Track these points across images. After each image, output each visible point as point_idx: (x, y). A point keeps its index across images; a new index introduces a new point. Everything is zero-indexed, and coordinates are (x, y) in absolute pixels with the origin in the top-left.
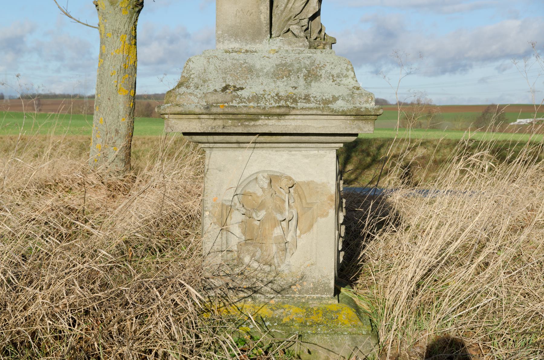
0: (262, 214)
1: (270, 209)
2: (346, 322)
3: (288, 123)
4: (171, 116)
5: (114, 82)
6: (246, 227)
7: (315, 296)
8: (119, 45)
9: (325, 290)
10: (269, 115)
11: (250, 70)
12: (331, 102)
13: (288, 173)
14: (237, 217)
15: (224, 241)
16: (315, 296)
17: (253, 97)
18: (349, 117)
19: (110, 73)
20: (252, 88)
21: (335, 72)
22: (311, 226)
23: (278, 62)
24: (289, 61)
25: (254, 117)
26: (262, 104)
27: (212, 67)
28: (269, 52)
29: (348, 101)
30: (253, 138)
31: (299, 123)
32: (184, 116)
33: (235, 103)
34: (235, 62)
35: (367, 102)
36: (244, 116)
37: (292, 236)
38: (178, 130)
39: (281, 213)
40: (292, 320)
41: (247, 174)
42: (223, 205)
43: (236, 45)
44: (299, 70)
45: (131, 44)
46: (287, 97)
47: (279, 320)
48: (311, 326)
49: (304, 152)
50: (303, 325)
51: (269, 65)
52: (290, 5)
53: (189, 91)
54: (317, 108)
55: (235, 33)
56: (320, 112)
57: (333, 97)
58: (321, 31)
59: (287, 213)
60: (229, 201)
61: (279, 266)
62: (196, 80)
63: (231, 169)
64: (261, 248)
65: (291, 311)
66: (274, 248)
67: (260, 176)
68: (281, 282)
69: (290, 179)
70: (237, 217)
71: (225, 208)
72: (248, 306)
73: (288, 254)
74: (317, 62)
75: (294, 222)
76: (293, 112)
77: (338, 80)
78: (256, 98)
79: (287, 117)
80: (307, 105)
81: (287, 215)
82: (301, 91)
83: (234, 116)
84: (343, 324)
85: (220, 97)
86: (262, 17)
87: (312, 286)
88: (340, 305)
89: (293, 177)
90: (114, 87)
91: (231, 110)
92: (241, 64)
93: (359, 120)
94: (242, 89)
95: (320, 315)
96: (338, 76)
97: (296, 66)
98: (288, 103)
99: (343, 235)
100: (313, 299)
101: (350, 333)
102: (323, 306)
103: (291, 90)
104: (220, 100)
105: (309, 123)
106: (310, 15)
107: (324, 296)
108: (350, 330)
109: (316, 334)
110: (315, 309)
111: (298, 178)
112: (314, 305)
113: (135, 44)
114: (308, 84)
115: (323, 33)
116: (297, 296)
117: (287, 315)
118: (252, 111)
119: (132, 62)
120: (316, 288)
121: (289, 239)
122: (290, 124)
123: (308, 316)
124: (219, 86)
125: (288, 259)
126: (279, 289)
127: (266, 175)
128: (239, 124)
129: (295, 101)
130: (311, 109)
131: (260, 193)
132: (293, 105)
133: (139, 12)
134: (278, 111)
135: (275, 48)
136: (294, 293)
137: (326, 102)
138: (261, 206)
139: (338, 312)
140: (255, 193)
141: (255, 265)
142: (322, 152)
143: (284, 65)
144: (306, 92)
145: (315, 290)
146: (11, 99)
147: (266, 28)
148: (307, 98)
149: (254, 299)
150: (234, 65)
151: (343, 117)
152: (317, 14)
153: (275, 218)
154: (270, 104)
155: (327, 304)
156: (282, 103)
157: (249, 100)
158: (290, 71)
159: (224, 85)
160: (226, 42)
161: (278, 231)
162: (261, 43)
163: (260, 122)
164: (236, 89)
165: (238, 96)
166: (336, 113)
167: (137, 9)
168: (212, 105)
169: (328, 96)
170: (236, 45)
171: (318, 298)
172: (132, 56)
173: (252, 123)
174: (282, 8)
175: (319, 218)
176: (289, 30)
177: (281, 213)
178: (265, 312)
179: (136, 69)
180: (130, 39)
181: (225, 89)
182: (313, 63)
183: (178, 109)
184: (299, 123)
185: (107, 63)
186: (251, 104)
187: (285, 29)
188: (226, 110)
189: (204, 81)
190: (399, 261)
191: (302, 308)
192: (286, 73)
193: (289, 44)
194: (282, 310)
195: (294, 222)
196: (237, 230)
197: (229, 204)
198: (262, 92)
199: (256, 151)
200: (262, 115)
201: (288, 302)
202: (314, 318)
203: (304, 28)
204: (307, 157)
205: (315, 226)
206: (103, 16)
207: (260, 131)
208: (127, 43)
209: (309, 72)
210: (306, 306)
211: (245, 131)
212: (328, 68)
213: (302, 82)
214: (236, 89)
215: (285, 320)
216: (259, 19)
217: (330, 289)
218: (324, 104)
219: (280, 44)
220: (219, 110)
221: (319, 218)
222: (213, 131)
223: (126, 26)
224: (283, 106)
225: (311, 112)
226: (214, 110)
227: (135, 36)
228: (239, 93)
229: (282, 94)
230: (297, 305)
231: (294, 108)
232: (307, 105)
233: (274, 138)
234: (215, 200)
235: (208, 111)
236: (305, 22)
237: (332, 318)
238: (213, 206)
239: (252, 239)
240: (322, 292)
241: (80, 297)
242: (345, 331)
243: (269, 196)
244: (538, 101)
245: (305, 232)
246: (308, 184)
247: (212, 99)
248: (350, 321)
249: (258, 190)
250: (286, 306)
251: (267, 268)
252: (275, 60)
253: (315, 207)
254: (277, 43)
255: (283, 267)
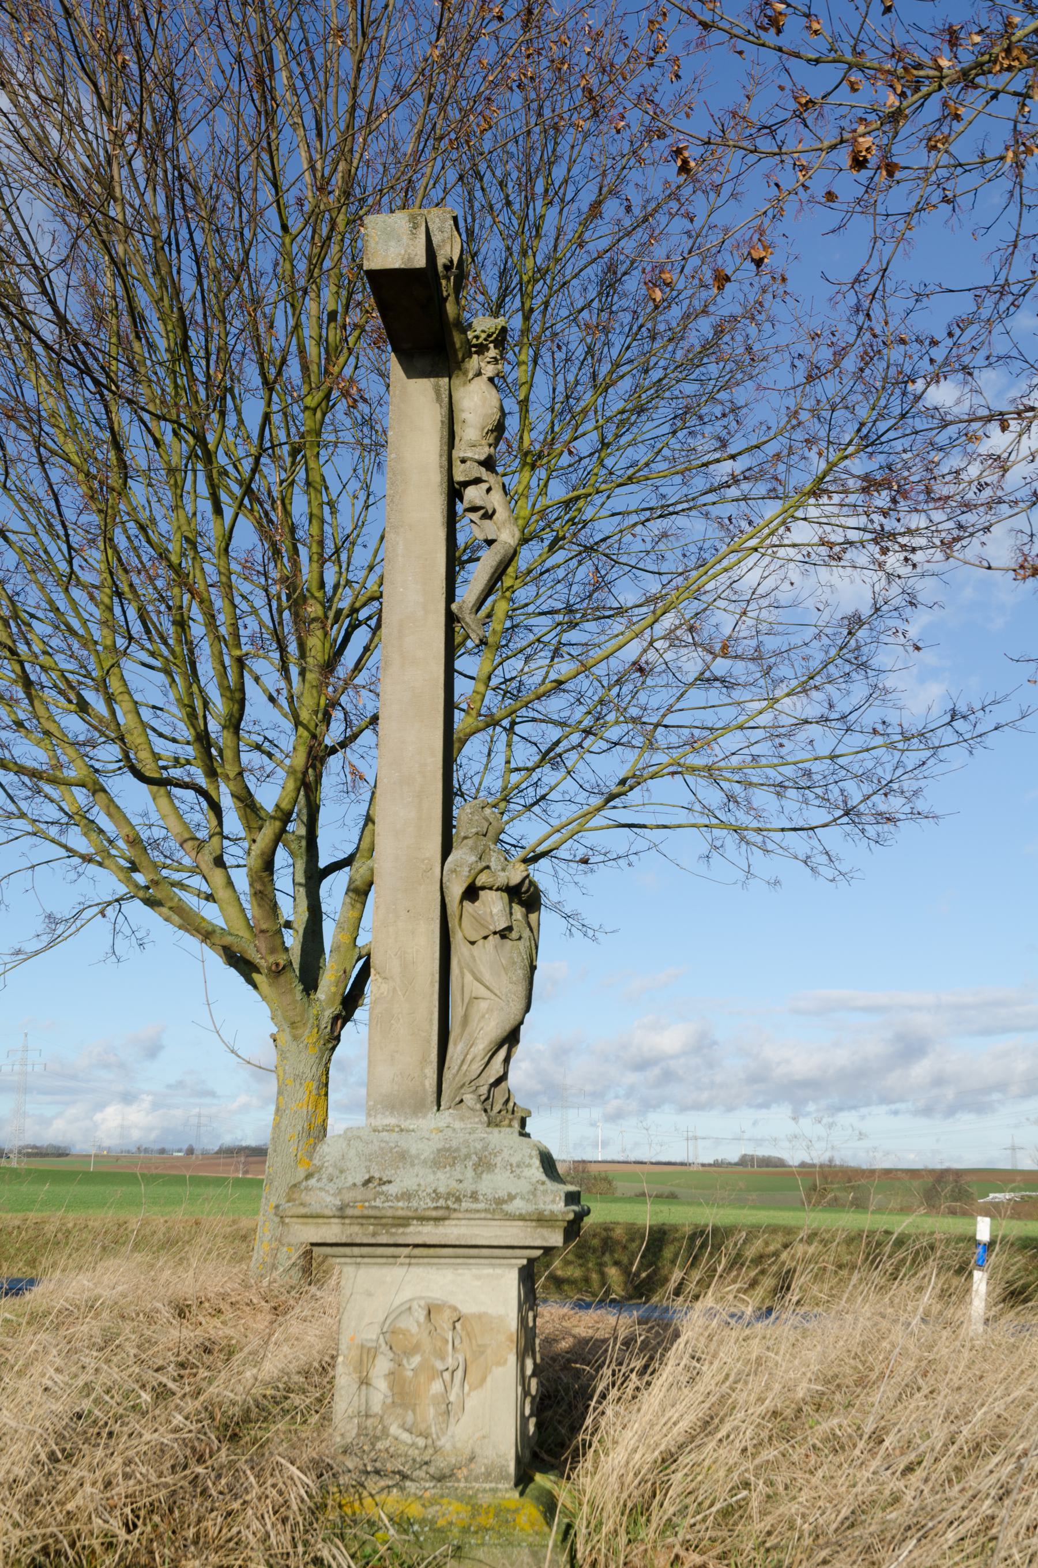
0: (416, 1360)
1: (433, 1354)
2: (527, 1527)
3: (448, 1230)
4: (294, 1220)
5: (292, 1149)
6: (394, 1378)
7: (488, 1486)
8: (303, 1094)
9: (503, 1477)
10: (422, 1219)
11: (403, 1157)
12: (504, 1202)
13: (453, 1301)
14: (382, 1365)
15: (363, 1400)
16: (488, 1486)
17: (403, 1194)
18: (529, 1223)
19: (288, 1137)
20: (404, 1180)
21: (514, 1160)
22: (483, 1379)
23: (440, 1146)
24: (454, 1144)
25: (403, 1222)
26: (414, 1204)
27: (352, 1153)
28: (433, 1129)
29: (528, 1200)
30: (406, 1251)
31: (463, 1230)
32: (310, 1220)
33: (378, 1203)
34: (383, 1145)
35: (553, 1201)
36: (390, 1221)
37: (458, 1395)
38: (302, 1240)
39: (443, 1358)
40: (451, 1523)
41: (397, 1303)
42: (362, 1346)
43: (391, 1121)
44: (467, 1157)
45: (319, 1095)
46: (449, 1194)
47: (433, 1522)
48: (476, 1532)
49: (475, 1271)
50: (465, 1530)
51: (426, 1149)
52: (465, 1067)
53: (319, 1185)
54: (486, 1211)
55: (392, 1104)
56: (490, 1216)
57: (509, 1194)
58: (507, 1101)
59: (450, 1359)
60: (371, 1340)
61: (439, 1438)
62: (330, 1170)
63: (373, 1296)
64: (414, 1411)
65: (451, 1508)
66: (432, 1411)
67: (415, 1305)
68: (440, 1464)
69: (455, 1309)
70: (382, 1365)
71: (365, 1351)
72: (393, 1500)
73: (452, 1420)
74: (491, 1146)
75: (459, 1374)
76: (454, 1215)
77: (518, 1171)
78: (407, 1196)
79: (447, 1222)
80: (475, 1206)
81: (450, 1362)
82: (468, 1186)
83: (378, 1220)
84: (522, 1530)
85: (359, 1194)
86: (427, 1083)
87: (483, 1470)
88: (522, 1500)
89: (460, 1307)
90: (293, 1158)
91: (371, 1212)
92: (392, 1148)
93: (542, 1227)
94: (390, 1182)
95: (491, 1515)
96: (518, 1166)
97: (464, 1151)
98: (449, 1203)
99: (533, 1392)
100: (485, 1491)
101: (530, 1545)
102: (496, 1501)
103: (454, 1184)
104: (359, 1198)
105: (476, 1231)
106: (492, 1080)
107: (500, 1486)
108: (531, 1539)
109: (483, 1544)
110: (485, 1506)
111: (467, 1308)
112: (485, 1499)
113: (326, 1094)
114: (479, 1176)
115: (511, 1104)
116: (462, 1485)
117: (444, 1515)
118: (400, 1213)
119: (320, 1120)
120: (489, 1474)
121: (452, 1398)
122: (451, 1232)
123: (473, 1517)
124: (360, 1178)
125: (451, 1428)
126: (437, 1475)
127: (422, 1303)
128: (385, 1233)
129: (458, 1200)
130: (478, 1211)
131: (414, 1329)
132: (456, 1206)
133: (333, 1049)
134: (434, 1214)
135: (442, 1124)
136: (458, 1480)
137: (500, 1202)
138: (416, 1349)
139: (517, 1511)
140: (409, 1331)
141: (405, 1436)
142: (499, 1271)
143: (448, 1150)
144: (473, 1187)
145: (487, 1476)
146: (205, 1153)
147: (432, 1097)
148: (474, 1196)
149: (402, 1489)
150: (382, 1149)
151: (521, 1223)
152: (502, 1079)
153: (433, 1367)
154: (424, 1204)
155: (504, 1498)
156: (441, 1203)
157: (397, 1198)
158: (455, 1158)
159: (367, 1177)
160: (379, 1116)
161: (437, 1387)
162: (424, 1117)
163: (411, 1229)
164: (382, 1182)
165: (382, 1193)
166: (510, 1217)
167: (330, 1046)
168: (348, 1205)
169: (502, 1194)
170: (391, 1121)
171: (491, 1490)
172: (320, 1111)
173: (401, 1230)
174: (454, 1071)
175: (494, 1368)
176: (462, 1101)
177: (443, 1358)
178: (415, 1510)
179: (325, 1130)
180: (318, 1088)
181: (369, 1181)
182: (485, 1148)
183: (303, 1211)
184: (463, 1230)
185: (285, 1122)
186: (400, 1204)
187: (458, 1099)
188: (366, 1212)
189: (342, 1172)
190: (628, 1434)
191: (467, 1504)
192: (450, 1160)
193: (462, 1119)
194: (438, 1508)
195: (459, 1374)
196: (381, 1385)
197: (374, 1344)
198: (415, 1187)
199: (412, 1269)
200: (413, 1218)
201: (448, 1495)
202: (482, 1520)
203: (483, 1098)
204: (478, 1277)
205: (489, 1379)
206: (282, 1054)
207: (410, 1242)
208: (314, 1092)
209: (480, 1159)
210: (473, 1501)
211: (391, 1242)
212: (505, 1154)
213: (470, 1173)
214: (382, 1182)
215: (441, 1523)
216: (424, 1085)
217: (509, 1475)
218: (497, 1204)
219: (450, 1120)
220: (357, 1212)
221: (494, 1368)
222: (349, 1241)
223: (314, 1069)
224: (441, 1208)
225: (477, 1216)
226: (349, 1212)
227: (327, 1085)
228: (385, 1188)
229: (442, 1190)
230: (460, 1499)
231: (455, 1210)
232: (475, 1206)
233: (432, 1251)
234: (352, 1339)
235: (341, 1214)
236: (484, 1090)
237: (507, 1521)
238: (349, 1348)
239: (403, 1395)
240: (497, 1480)
241: (140, 1483)
242: (523, 1540)
243: (425, 1334)
244: (1026, 1163)
245: (476, 1388)
246: (480, 1316)
247: (348, 1196)
248: (532, 1525)
249: (413, 1324)
250: (445, 1501)
251: (421, 1442)
252: (437, 1142)
253: (489, 1351)
254: (446, 1117)
255: (443, 1442)
